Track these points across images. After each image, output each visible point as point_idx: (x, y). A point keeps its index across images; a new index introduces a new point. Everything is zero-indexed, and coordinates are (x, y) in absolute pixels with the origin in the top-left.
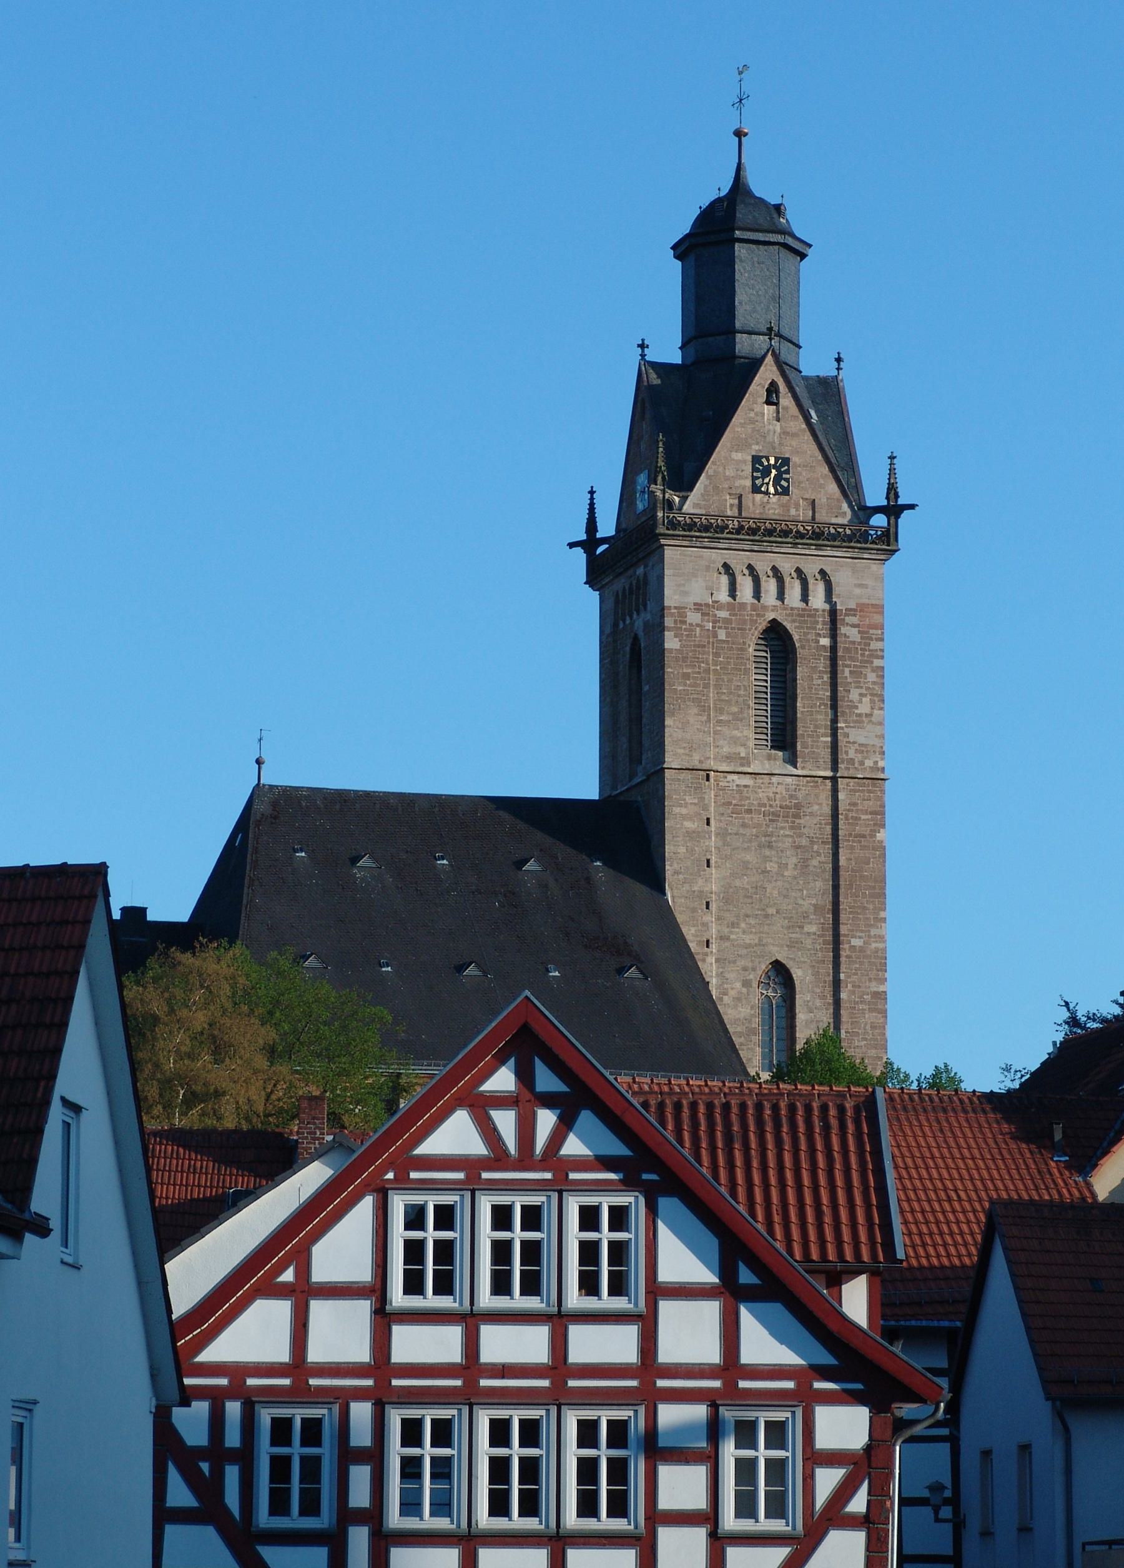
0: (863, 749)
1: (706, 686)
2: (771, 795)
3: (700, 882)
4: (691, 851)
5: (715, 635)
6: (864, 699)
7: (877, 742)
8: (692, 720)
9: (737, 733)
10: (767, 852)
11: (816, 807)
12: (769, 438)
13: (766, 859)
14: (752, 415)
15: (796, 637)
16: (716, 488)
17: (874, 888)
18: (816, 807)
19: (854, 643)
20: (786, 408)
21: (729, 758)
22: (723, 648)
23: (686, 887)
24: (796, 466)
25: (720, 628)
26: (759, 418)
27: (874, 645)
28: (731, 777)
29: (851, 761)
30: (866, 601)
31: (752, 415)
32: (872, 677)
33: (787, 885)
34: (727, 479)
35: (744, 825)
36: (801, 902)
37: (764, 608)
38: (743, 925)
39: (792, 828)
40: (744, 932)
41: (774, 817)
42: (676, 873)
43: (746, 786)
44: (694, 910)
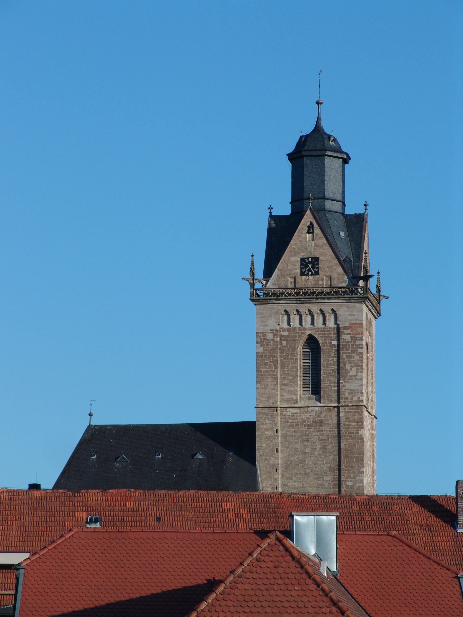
0: (353, 392)
1: (276, 368)
2: (308, 416)
3: (273, 460)
4: (268, 445)
5: (281, 344)
6: (353, 368)
7: (359, 388)
8: (269, 384)
9: (292, 389)
10: (306, 443)
11: (330, 421)
12: (309, 249)
13: (306, 447)
14: (300, 239)
15: (320, 342)
16: (283, 275)
17: (358, 457)
18: (330, 421)
19: (348, 342)
20: (317, 234)
21: (288, 401)
22: (285, 350)
23: (266, 462)
24: (322, 261)
25: (283, 340)
26: (304, 240)
27: (358, 342)
28: (288, 410)
29: (347, 398)
30: (354, 322)
31: (300, 239)
32: (357, 358)
33: (316, 459)
34: (288, 270)
35: (295, 432)
36: (322, 466)
37: (305, 329)
38: (294, 478)
39: (318, 431)
40: (295, 482)
41: (309, 427)
42: (261, 456)
43: (296, 413)
44: (270, 473)
